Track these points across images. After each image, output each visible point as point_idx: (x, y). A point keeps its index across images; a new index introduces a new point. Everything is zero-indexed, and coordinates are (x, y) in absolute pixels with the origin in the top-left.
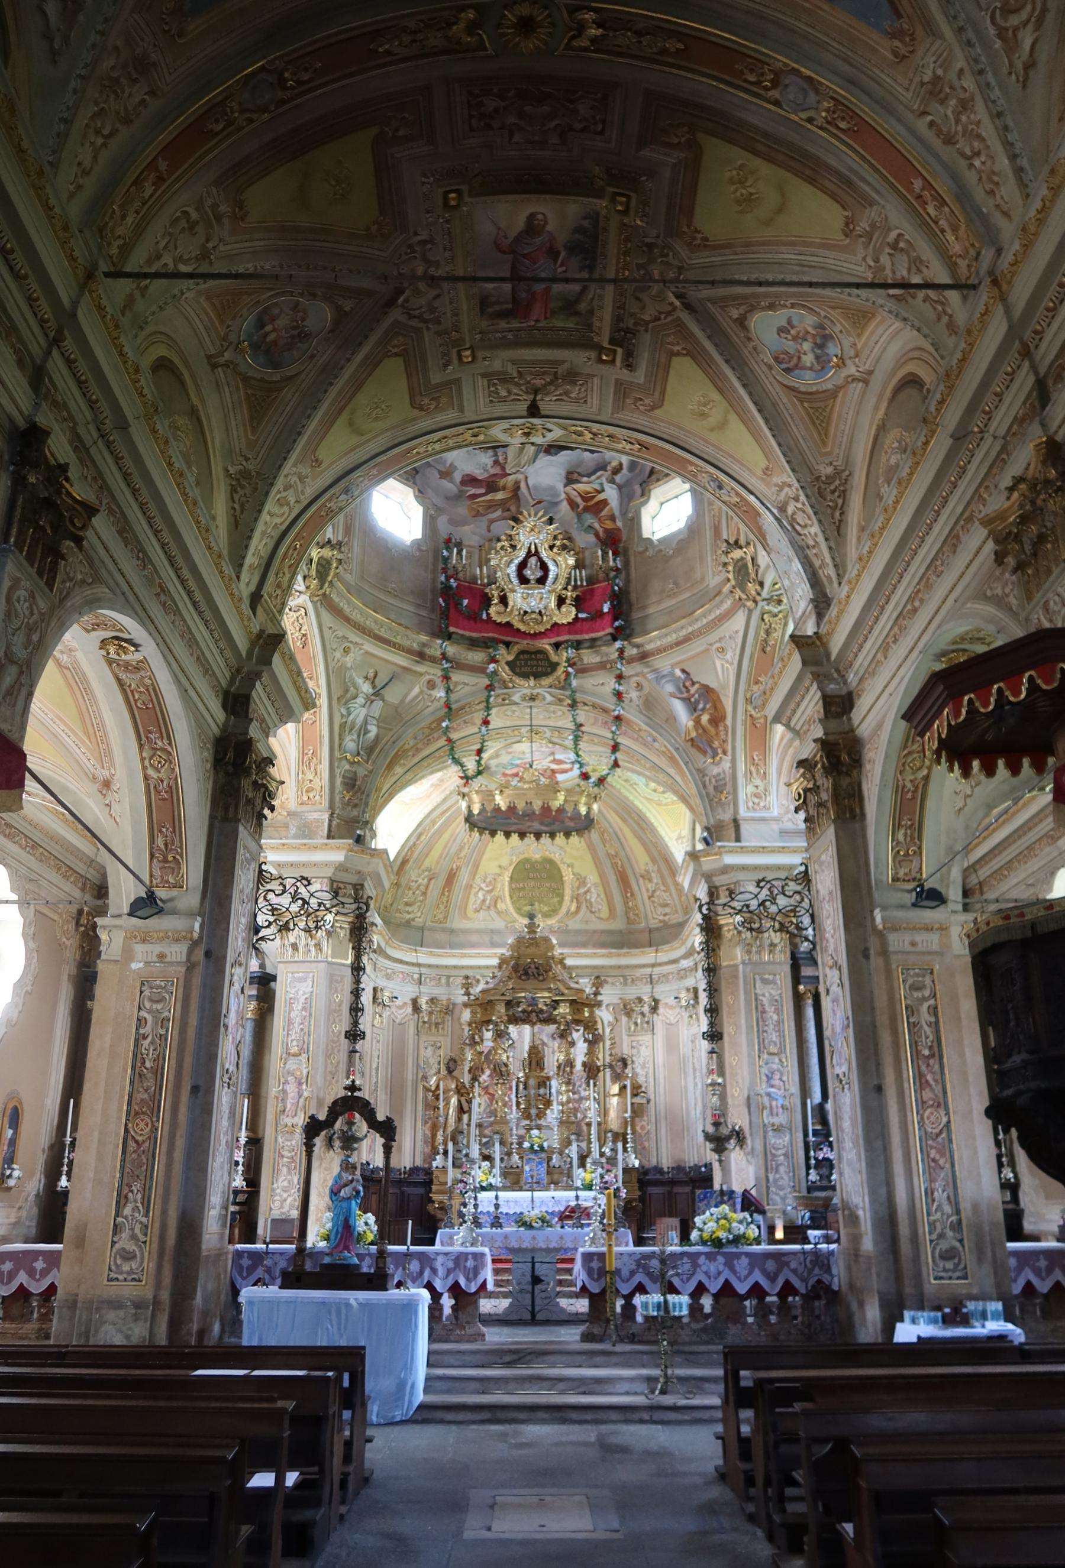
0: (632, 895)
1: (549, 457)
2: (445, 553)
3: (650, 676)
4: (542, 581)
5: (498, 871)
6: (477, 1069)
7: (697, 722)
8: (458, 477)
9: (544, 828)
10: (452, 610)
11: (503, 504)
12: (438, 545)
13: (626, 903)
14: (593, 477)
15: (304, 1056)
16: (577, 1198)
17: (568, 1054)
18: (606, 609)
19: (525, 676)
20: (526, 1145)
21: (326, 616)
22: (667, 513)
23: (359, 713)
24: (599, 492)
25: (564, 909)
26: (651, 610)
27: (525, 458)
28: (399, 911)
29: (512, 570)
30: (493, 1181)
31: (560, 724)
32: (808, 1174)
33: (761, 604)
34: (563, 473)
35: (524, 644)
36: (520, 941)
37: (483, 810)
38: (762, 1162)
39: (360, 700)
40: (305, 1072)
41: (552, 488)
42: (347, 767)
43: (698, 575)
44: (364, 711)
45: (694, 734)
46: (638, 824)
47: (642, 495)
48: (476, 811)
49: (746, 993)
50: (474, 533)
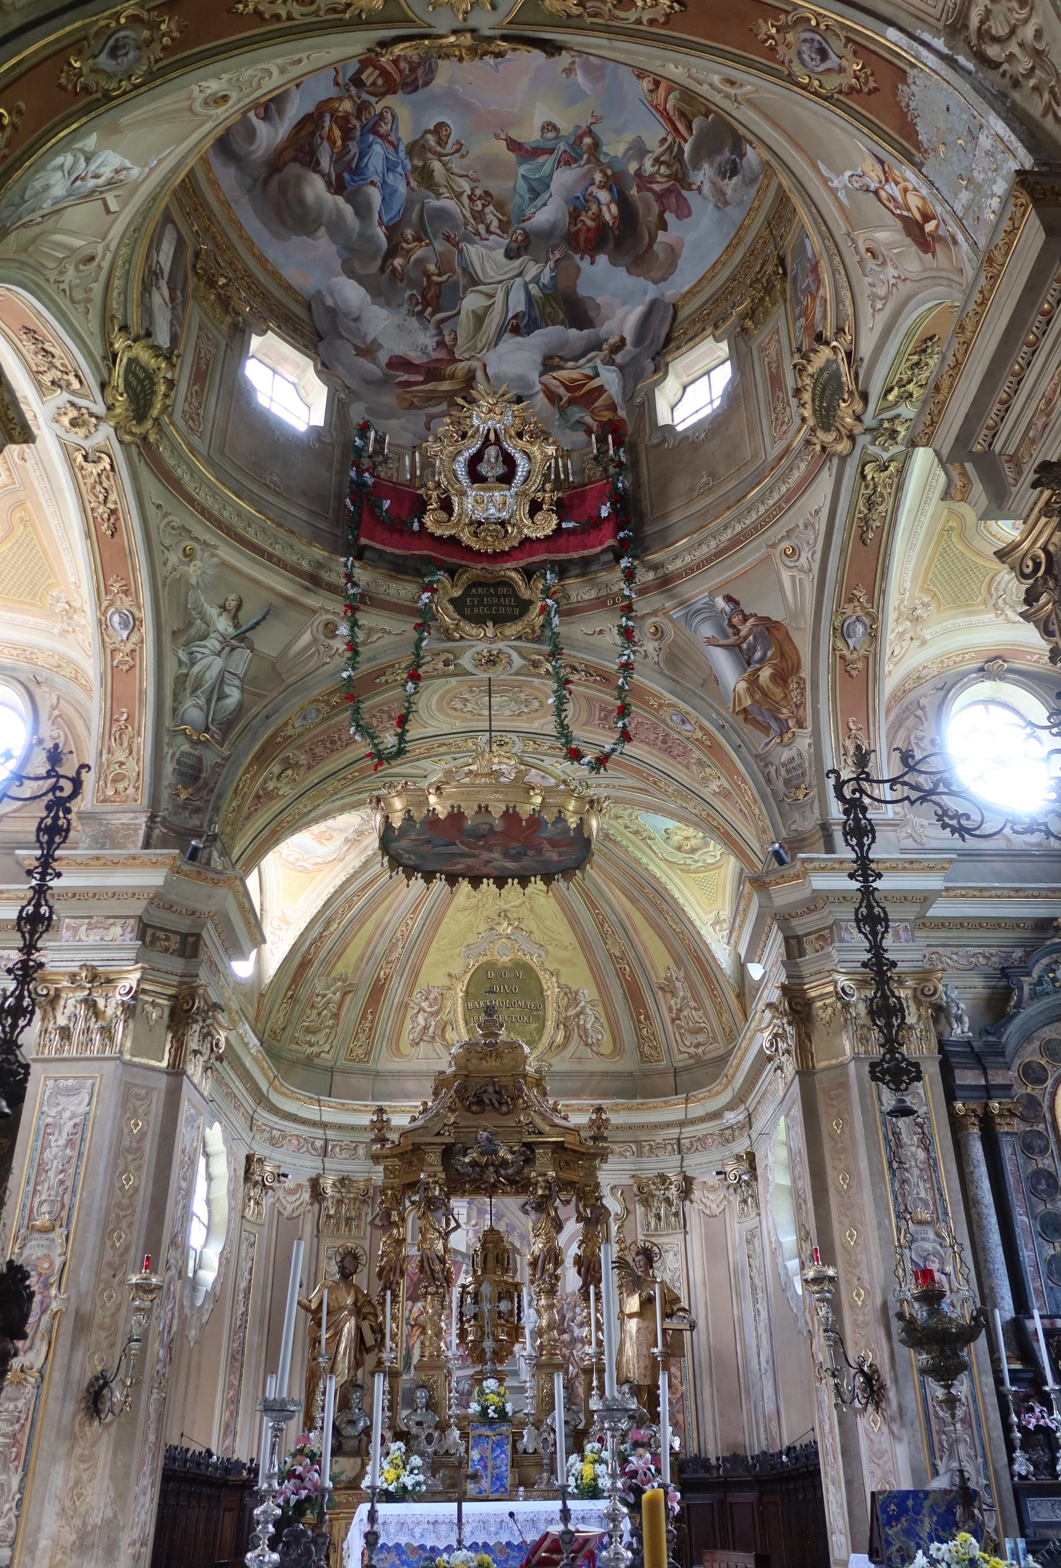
0: (647, 1017)
1: (519, 339)
2: (358, 442)
3: (676, 614)
4: (507, 478)
5: (446, 982)
6: (392, 1269)
7: (753, 682)
8: (383, 357)
9: (510, 865)
10: (365, 515)
11: (448, 397)
12: (346, 437)
13: (638, 1031)
14: (582, 361)
15: (60, 1231)
16: (565, 1515)
17: (550, 1240)
18: (604, 513)
19: (479, 620)
20: (474, 1407)
21: (145, 474)
22: (693, 393)
23: (210, 664)
24: (591, 378)
25: (546, 1040)
26: (675, 518)
27: (483, 339)
28: (294, 1040)
29: (460, 467)
30: (409, 1481)
31: (535, 726)
32: (1011, 1461)
33: (863, 440)
34: (539, 359)
35: (477, 570)
36: (469, 1047)
37: (409, 818)
38: (921, 1436)
39: (213, 643)
40: (58, 1262)
41: (522, 379)
42: (186, 747)
43: (748, 454)
44: (218, 663)
45: (748, 702)
46: (654, 905)
47: (656, 371)
48: (397, 824)
49: (864, 1111)
50: (405, 429)
